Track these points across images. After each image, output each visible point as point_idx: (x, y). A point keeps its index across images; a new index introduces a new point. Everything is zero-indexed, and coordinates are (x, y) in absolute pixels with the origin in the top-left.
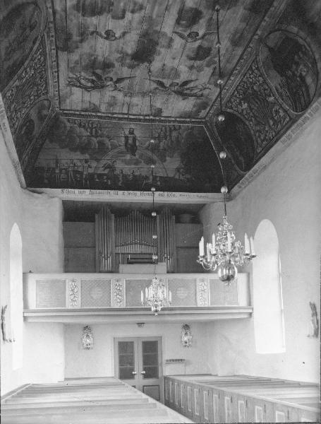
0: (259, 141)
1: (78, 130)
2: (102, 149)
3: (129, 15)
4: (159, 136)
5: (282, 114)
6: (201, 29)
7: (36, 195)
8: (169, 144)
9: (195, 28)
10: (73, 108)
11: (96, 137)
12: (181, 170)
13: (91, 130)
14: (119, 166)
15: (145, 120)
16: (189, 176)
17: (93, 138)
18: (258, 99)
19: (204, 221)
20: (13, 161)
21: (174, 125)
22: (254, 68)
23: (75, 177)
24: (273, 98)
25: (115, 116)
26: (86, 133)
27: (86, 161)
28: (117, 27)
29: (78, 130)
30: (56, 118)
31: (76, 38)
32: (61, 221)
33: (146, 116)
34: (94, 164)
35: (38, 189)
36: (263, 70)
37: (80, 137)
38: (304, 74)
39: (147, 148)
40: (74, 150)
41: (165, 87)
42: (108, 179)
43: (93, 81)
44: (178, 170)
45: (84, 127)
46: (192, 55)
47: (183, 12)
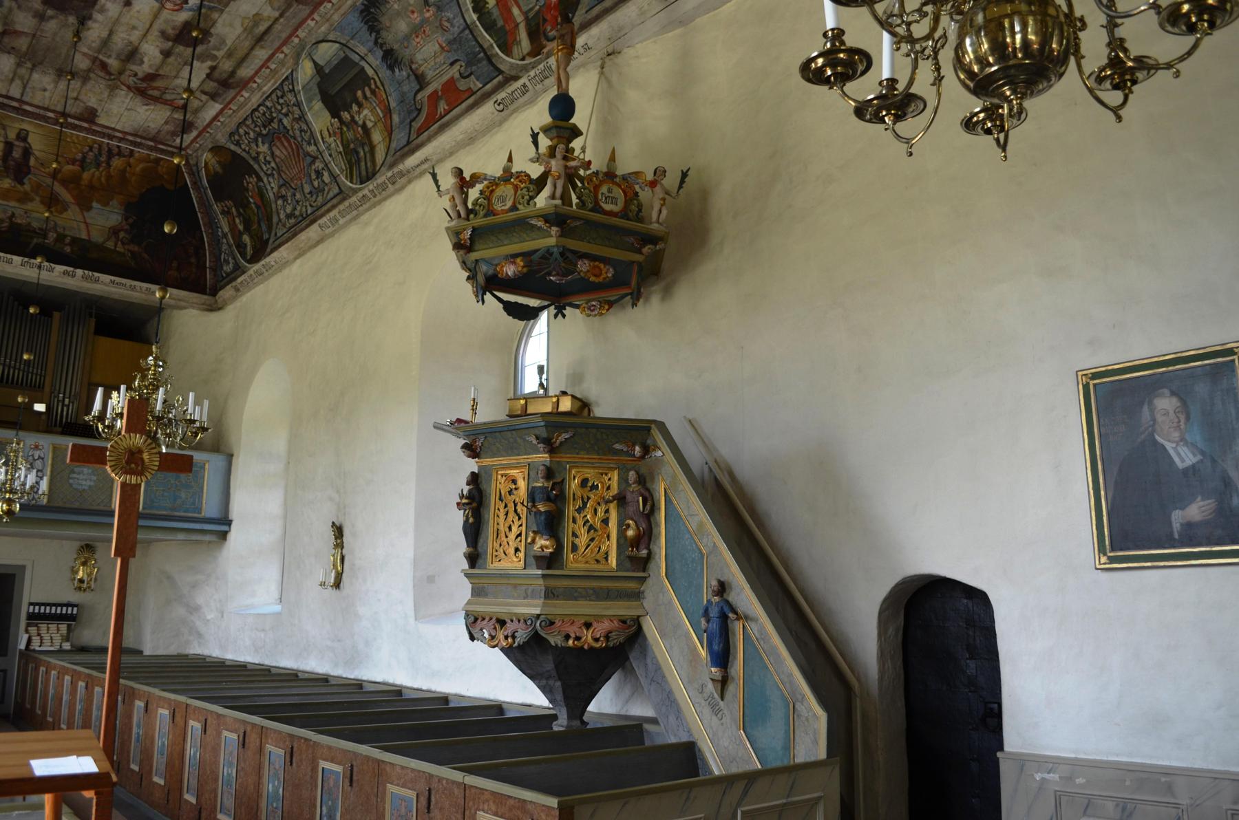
0: (282, 216)
4: (84, 158)
12: (122, 235)
18: (289, 141)
21: (118, 147)
22: (286, 88)
38: (370, 125)
41: (110, 74)
44: (114, 231)
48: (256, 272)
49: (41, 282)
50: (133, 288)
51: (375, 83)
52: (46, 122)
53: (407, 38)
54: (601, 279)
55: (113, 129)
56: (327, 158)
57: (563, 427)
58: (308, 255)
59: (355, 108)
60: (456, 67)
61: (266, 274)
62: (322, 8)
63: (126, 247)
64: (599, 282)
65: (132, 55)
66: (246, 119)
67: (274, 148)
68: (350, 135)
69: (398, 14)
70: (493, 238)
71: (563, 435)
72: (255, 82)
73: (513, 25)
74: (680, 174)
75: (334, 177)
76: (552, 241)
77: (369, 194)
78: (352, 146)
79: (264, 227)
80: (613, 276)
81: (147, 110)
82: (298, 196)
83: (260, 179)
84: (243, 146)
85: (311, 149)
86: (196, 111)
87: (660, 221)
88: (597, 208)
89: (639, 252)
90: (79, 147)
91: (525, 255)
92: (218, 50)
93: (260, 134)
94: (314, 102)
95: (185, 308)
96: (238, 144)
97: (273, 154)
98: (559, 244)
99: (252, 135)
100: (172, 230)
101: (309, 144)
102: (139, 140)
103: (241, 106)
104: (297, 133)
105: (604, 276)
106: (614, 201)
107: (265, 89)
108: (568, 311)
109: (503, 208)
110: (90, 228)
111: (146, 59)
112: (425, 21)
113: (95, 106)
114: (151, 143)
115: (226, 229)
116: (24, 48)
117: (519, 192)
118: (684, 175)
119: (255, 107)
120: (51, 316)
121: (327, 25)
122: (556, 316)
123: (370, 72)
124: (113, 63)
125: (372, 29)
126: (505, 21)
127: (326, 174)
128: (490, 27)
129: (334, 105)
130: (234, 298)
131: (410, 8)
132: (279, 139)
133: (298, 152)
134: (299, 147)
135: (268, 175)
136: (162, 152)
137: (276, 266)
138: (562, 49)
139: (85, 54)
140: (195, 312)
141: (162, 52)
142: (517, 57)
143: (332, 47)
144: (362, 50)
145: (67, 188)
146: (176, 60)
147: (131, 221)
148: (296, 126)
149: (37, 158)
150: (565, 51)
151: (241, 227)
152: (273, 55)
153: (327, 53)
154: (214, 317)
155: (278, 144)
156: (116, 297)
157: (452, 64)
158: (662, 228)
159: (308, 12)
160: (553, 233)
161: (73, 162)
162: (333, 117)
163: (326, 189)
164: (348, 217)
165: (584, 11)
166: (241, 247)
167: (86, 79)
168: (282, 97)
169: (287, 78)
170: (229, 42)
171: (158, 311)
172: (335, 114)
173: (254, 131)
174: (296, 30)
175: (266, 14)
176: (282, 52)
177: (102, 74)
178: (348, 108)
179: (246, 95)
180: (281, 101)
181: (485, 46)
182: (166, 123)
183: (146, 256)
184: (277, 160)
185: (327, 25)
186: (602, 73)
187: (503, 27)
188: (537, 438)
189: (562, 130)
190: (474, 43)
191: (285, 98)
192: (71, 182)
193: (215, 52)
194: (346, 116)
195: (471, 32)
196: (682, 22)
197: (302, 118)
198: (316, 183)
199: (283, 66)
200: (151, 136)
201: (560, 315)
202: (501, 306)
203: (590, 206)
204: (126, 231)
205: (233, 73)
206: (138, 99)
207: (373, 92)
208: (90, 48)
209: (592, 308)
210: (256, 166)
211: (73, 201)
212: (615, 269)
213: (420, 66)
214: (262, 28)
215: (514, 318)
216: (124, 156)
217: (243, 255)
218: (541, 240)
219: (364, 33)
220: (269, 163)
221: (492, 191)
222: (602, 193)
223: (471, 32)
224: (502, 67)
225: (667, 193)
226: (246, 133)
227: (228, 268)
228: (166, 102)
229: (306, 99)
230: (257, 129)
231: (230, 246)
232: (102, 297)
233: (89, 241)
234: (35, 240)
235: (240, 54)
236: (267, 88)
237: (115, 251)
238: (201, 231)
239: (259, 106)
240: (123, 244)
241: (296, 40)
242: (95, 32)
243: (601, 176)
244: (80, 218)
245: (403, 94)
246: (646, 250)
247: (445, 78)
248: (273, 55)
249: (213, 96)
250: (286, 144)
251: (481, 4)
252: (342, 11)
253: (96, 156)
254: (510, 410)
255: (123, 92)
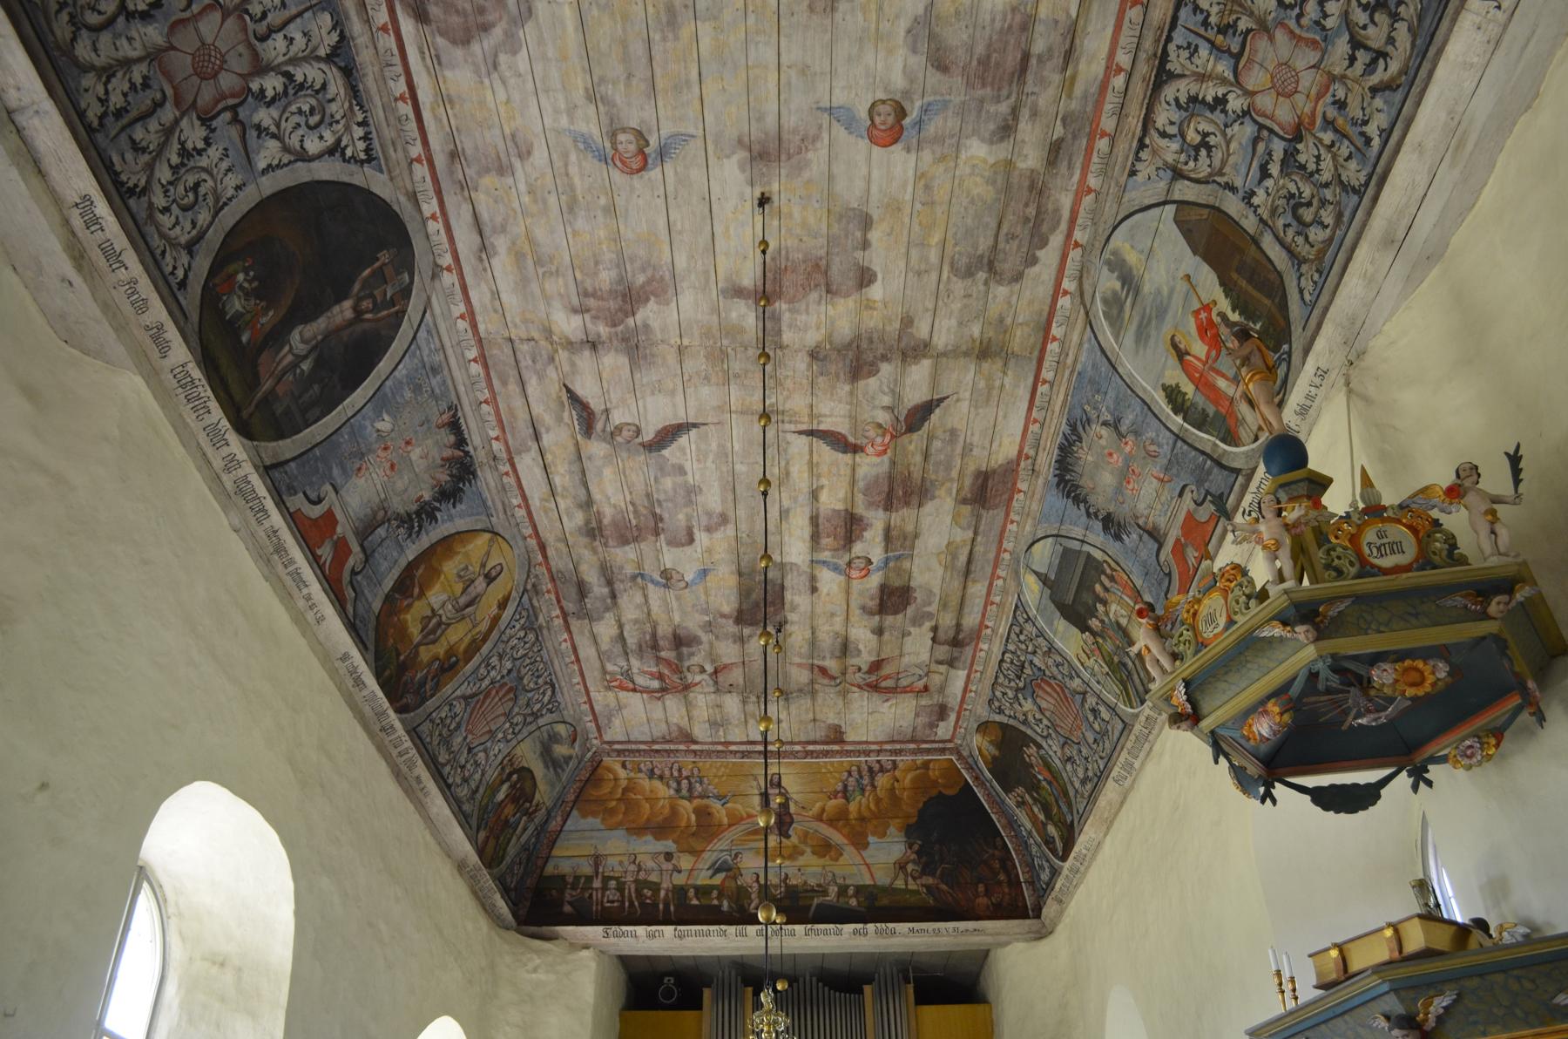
0: (1077, 785)
1: (645, 783)
2: (706, 827)
3: (701, 537)
4: (845, 786)
5: (1105, 714)
6: (871, 546)
7: (537, 943)
8: (872, 806)
9: (858, 549)
10: (632, 739)
11: (690, 798)
12: (910, 867)
13: (679, 783)
14: (751, 864)
15: (808, 754)
16: (930, 880)
17: (685, 803)
18: (1049, 685)
19: (991, 996)
20: (461, 866)
21: (878, 762)
22: (1021, 620)
23: (639, 893)
24: (1077, 681)
25: (733, 748)
26: (664, 791)
27: (669, 856)
28: (685, 562)
29: (645, 783)
30: (597, 765)
31: (598, 589)
32: (616, 1011)
33: (809, 743)
34: (685, 862)
35: (545, 929)
36: (1041, 622)
37: (652, 800)
38: (1124, 622)
39: (819, 818)
40: (638, 831)
41: (833, 678)
42: (720, 897)
43: (661, 677)
44: (901, 866)
45: (661, 778)
46: (873, 604)
47: (821, 521)
48: (1071, 870)
49: (785, 952)
50: (937, 932)
51: (1109, 565)
52: (795, 757)
53: (1119, 490)
54: (1427, 688)
55: (867, 742)
56: (1097, 687)
57: (1433, 985)
58: (1116, 824)
59: (1100, 607)
60: (1188, 496)
61: (1082, 869)
62: (1015, 503)
63: (918, 881)
64: (1427, 694)
65: (845, 648)
66: (996, 677)
67: (1038, 700)
68: (1108, 646)
69: (1097, 466)
70: (1222, 685)
71: (1436, 1001)
72: (987, 627)
73: (1227, 403)
74: (1506, 463)
75: (1112, 709)
76: (1309, 653)
77: (1152, 713)
78: (1116, 659)
79: (1065, 809)
80: (1449, 674)
81: (890, 707)
82: (1084, 751)
83: (1039, 747)
84: (1007, 712)
85: (1076, 684)
86: (942, 689)
87: (1502, 550)
88: (1367, 569)
89: (1485, 616)
90: (837, 775)
91: (1278, 693)
92: (930, 604)
93: (1018, 690)
94: (1055, 623)
95: (1007, 944)
96: (1001, 711)
97: (1040, 710)
98: (1324, 653)
99: (1011, 694)
100: (768, 822)
101: (1071, 678)
102: (898, 746)
103: (986, 663)
104: (1054, 669)
105: (1430, 679)
106: (1396, 547)
107: (1001, 630)
108: (1434, 772)
109: (1216, 631)
110: (873, 870)
111: (861, 647)
112: (1128, 459)
113: (836, 722)
114: (912, 746)
115: (1029, 825)
116: (741, 681)
117: (1230, 596)
118: (1515, 460)
119: (1000, 657)
120: (861, 992)
121: (1030, 521)
122: (1415, 788)
123: (1098, 555)
124: (831, 664)
125: (1078, 500)
126: (1216, 403)
127: (1102, 709)
128: (1201, 423)
129: (1077, 616)
130: (1061, 913)
131: (1106, 451)
132: (1039, 686)
133: (1064, 694)
134: (1063, 687)
135: (1045, 738)
136: (928, 751)
137: (1089, 855)
138: (1250, 380)
139: (800, 665)
140: (1020, 946)
141: (873, 632)
142: (1248, 441)
143: (1045, 546)
144: (1077, 532)
145: (835, 828)
146: (891, 634)
147: (916, 847)
148: (1050, 662)
149: (796, 802)
150: (1257, 377)
151: (1042, 817)
152: (991, 585)
153: (1044, 555)
154: (1044, 946)
155: (1041, 693)
156: (922, 949)
157: (1181, 495)
158: (1505, 560)
159: (1002, 514)
160: (1302, 637)
161: (835, 795)
162: (1083, 632)
163: (1109, 728)
164: (1142, 755)
165: (1300, 330)
166: (1049, 842)
167: (813, 694)
168: (1021, 632)
169: (1017, 606)
170: (937, 590)
171: (983, 956)
172: (1084, 628)
173: (1011, 688)
174: (1001, 542)
175: (958, 539)
176: (999, 577)
177: (826, 681)
178: (1092, 612)
179: (985, 647)
180: (1022, 638)
181: (1208, 450)
182: (917, 715)
183: (944, 887)
184: (1047, 714)
185: (1030, 521)
186: (1350, 392)
187: (1217, 413)
188: (1388, 1018)
189: (1293, 486)
190: (1193, 453)
191: (1025, 632)
192: (838, 819)
193: (928, 609)
194: (1094, 623)
195: (1185, 441)
196: (1433, 256)
197: (1051, 649)
198: (1096, 726)
199: (1007, 593)
200: (908, 737)
201: (1422, 784)
202: (1308, 798)
203: (1353, 570)
204: (914, 861)
205: (958, 626)
206: (875, 696)
207: (1112, 579)
208: (800, 655)
209: (1469, 752)
210: (1029, 732)
211: (846, 842)
212: (1447, 661)
213: (1147, 518)
214: (963, 558)
215: (1337, 812)
216: (888, 771)
217: (1054, 851)
218: (1293, 658)
219: (1072, 510)
220: (1041, 721)
221: (1195, 614)
222: (1369, 544)
223: (1185, 441)
224: (1236, 465)
225: (1496, 500)
226: (1004, 694)
227: (1045, 876)
228: (905, 690)
229: (1046, 623)
230: (1013, 684)
231: (1039, 846)
232: (951, 952)
233: (875, 886)
234: (816, 901)
235: (954, 602)
236: (1003, 630)
237: (907, 891)
238: (1002, 837)
239: (1003, 654)
240: (914, 879)
241: (1006, 556)
242: (797, 635)
243: (1355, 518)
244: (858, 860)
245: (1144, 564)
246: (1493, 608)
247: (1181, 517)
248: (991, 585)
249: (951, 663)
250: (1049, 690)
251: (1180, 400)
252: (1037, 496)
253: (857, 781)
254: (1319, 975)
255: (856, 694)
